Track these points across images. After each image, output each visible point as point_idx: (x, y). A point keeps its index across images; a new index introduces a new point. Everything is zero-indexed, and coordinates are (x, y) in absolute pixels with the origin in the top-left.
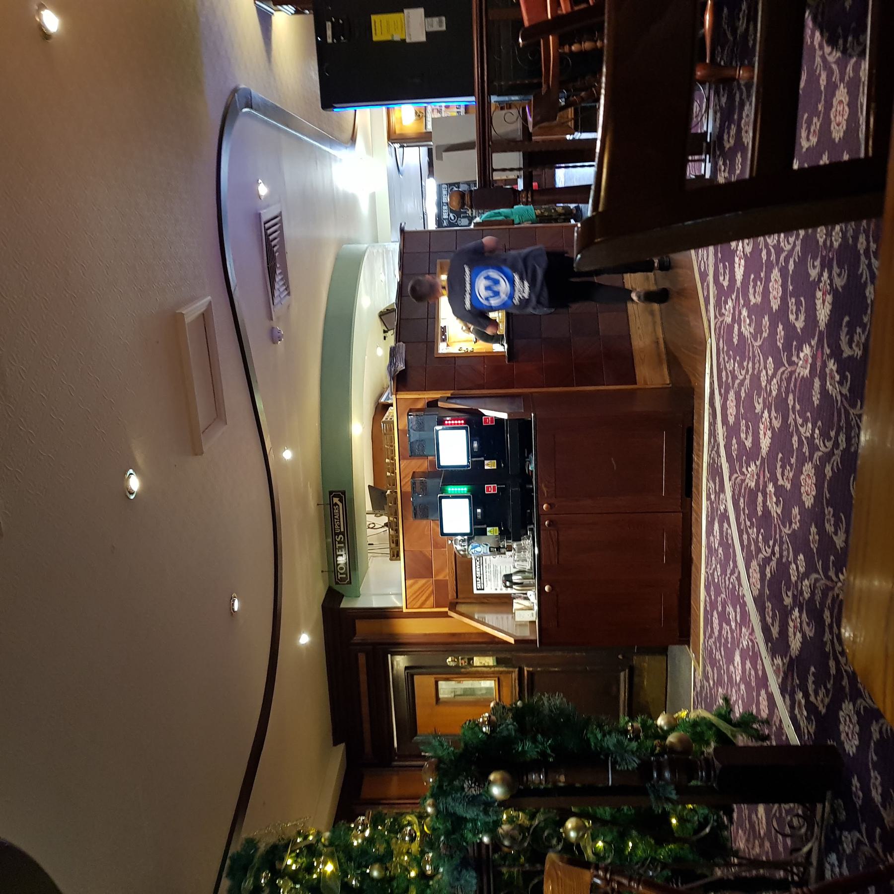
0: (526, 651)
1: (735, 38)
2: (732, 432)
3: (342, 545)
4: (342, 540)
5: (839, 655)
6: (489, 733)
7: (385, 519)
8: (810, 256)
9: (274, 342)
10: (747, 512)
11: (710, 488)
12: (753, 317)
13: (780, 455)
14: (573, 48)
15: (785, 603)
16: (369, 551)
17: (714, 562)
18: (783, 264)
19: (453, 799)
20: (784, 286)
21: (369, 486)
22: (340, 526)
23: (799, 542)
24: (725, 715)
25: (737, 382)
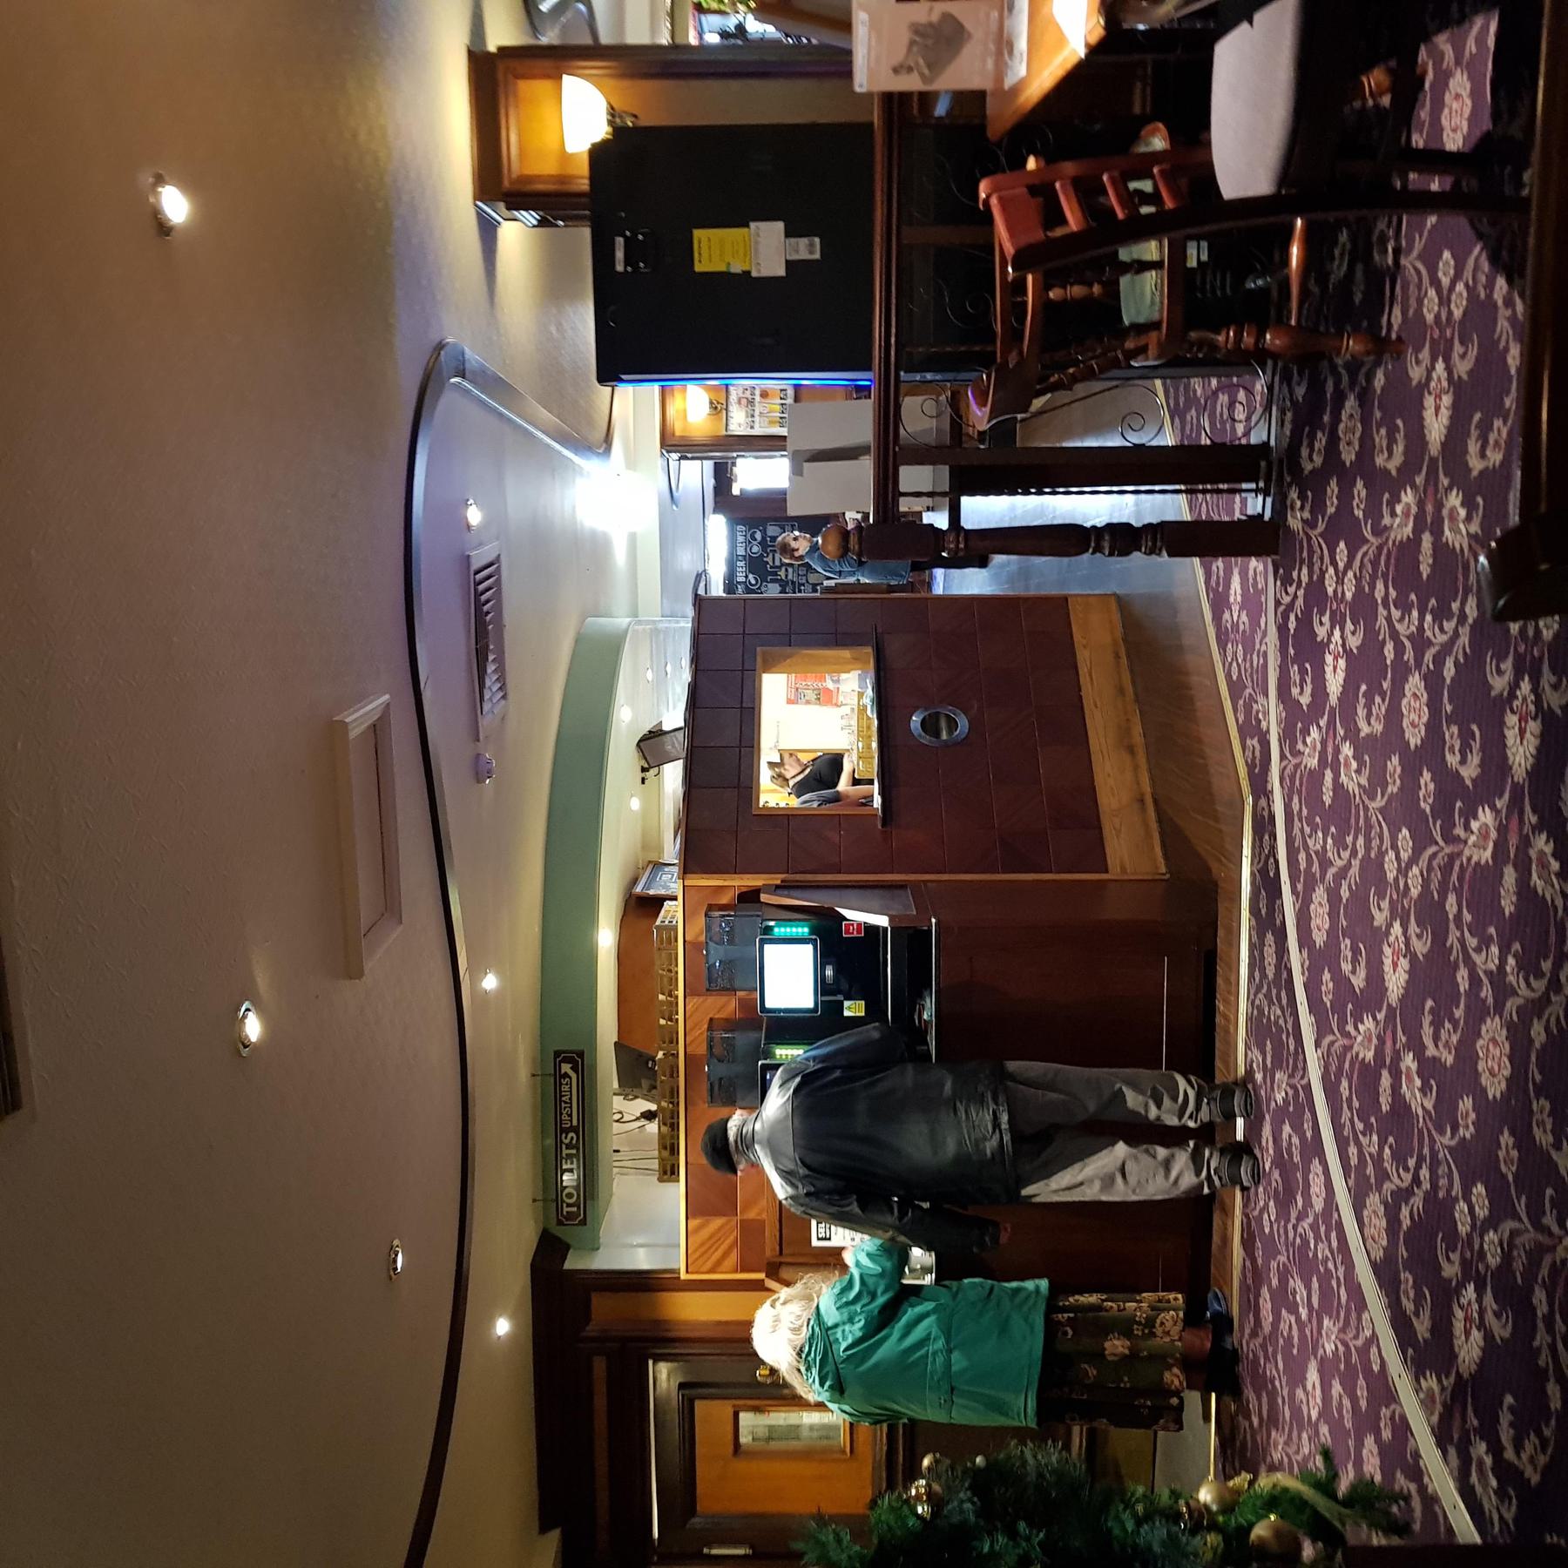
1: (1324, 289)
2: (1321, 959)
3: (574, 1151)
4: (574, 1142)
5: (1360, 1136)
6: (929, 1517)
8: (1489, 654)
9: (479, 779)
10: (1356, 1104)
11: (1252, 1061)
12: (1367, 758)
13: (1429, 1003)
14: (1051, 295)
15: (1445, 1274)
18: (1431, 666)
20: (1434, 705)
22: (570, 1115)
24: (1326, 1486)
25: (1331, 872)
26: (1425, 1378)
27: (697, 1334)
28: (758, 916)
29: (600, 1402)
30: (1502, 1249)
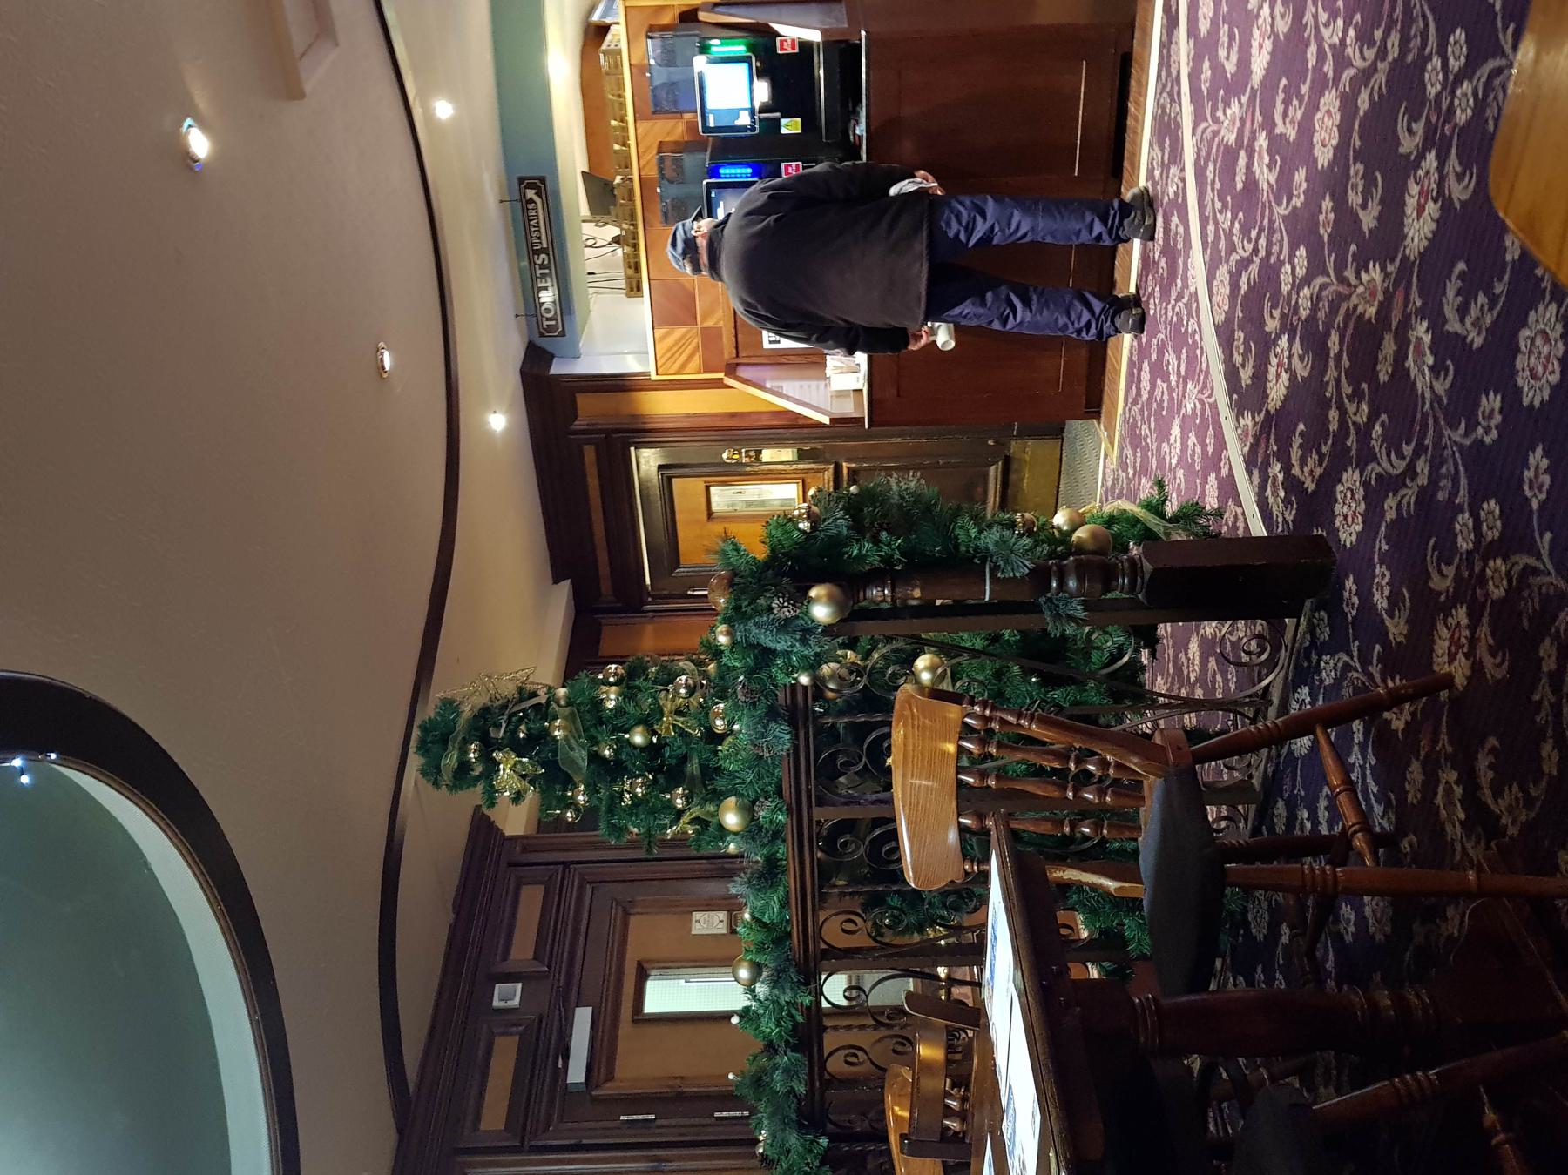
0: (847, 437)
2: (1204, 47)
3: (547, 271)
4: (546, 262)
5: (1346, 401)
7: (613, 231)
11: (1153, 159)
13: (1284, 82)
15: (1267, 329)
16: (590, 285)
17: (1150, 283)
19: (756, 624)
21: (583, 172)
23: (1302, 229)
24: (1156, 508)
28: (696, 35)
29: (593, 483)
30: (1510, 581)
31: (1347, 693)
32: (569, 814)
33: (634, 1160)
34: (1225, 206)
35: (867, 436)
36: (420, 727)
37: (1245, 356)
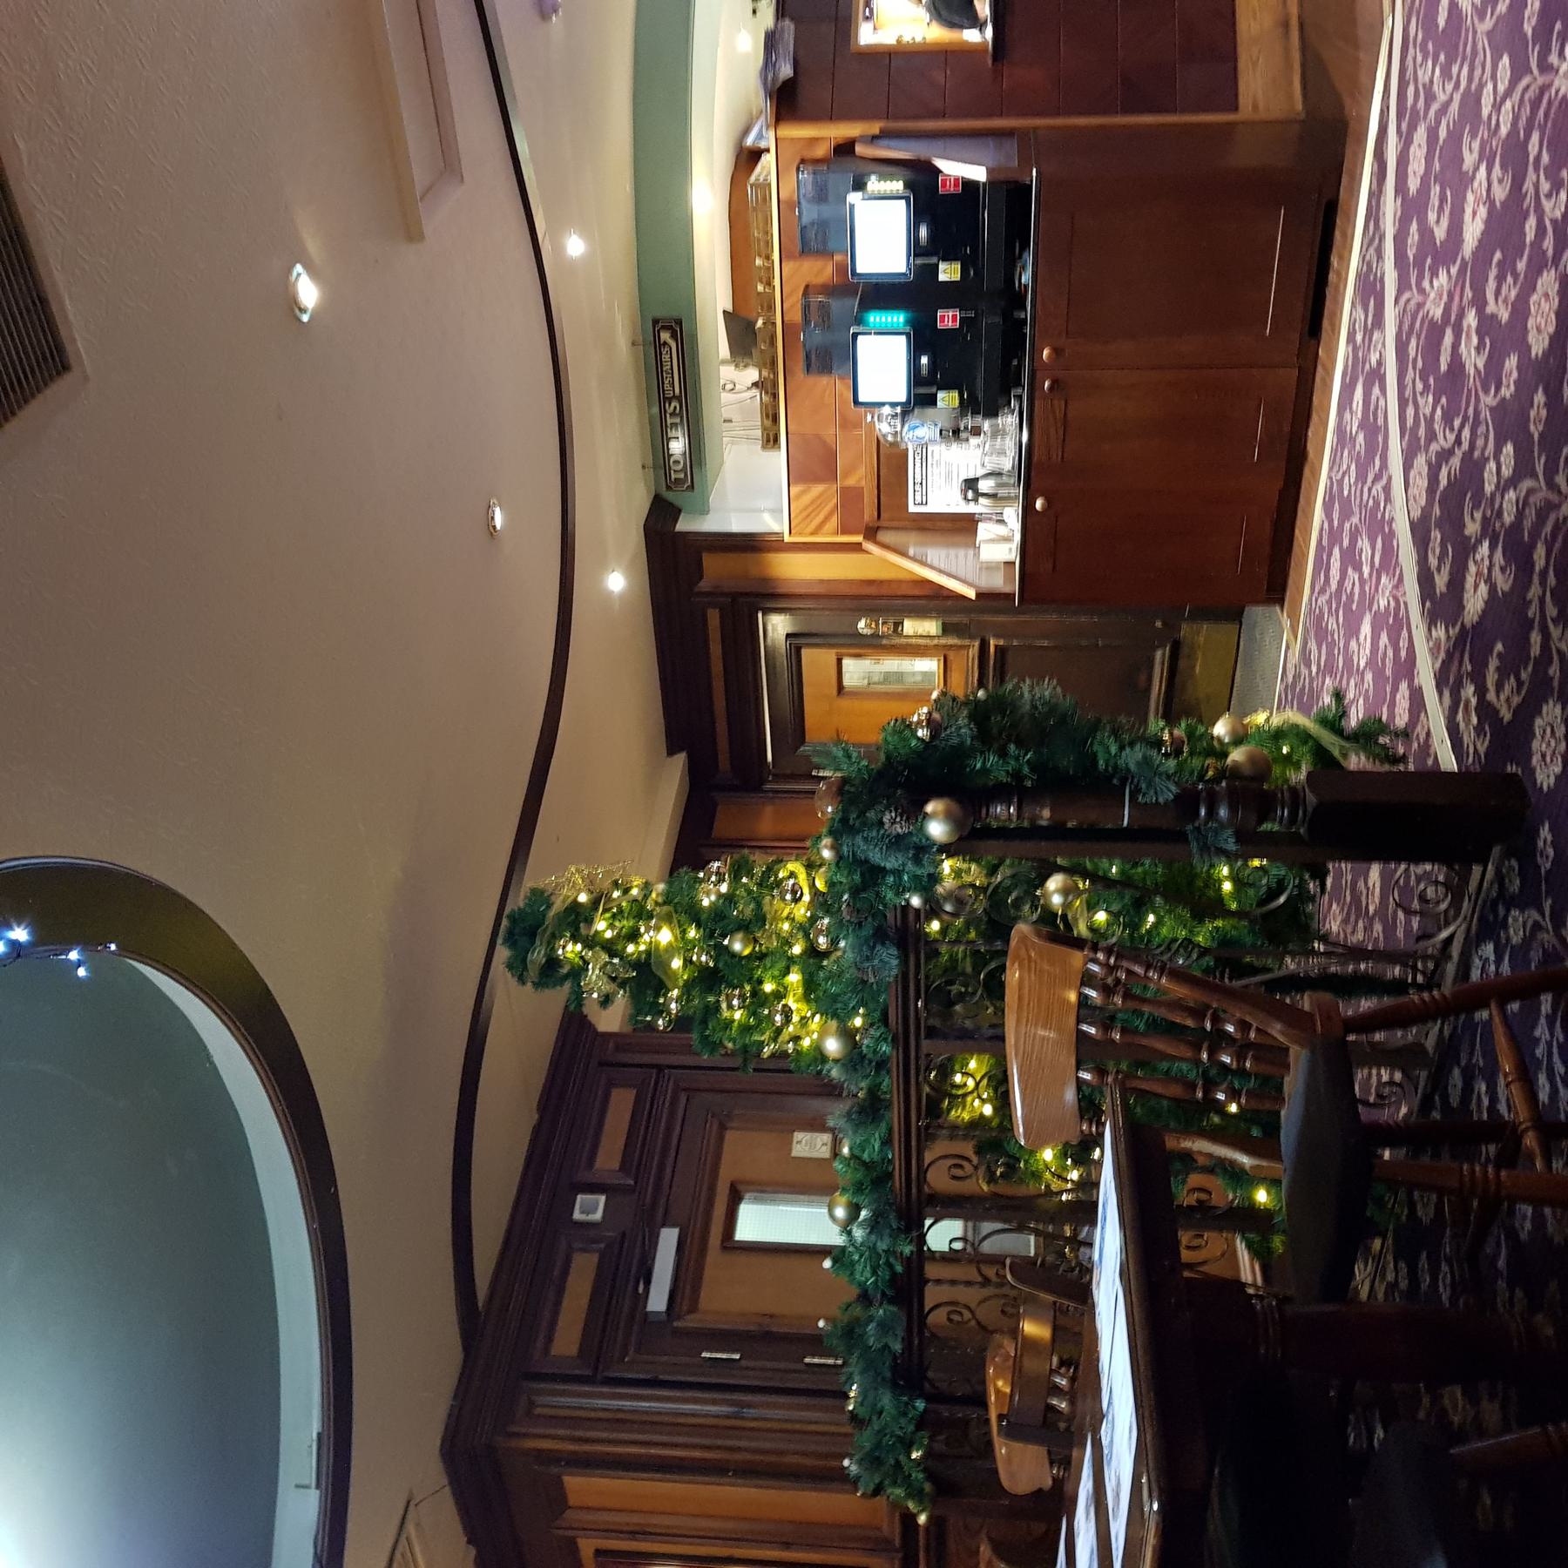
2: (1413, 208)
3: (678, 420)
7: (752, 374)
13: (1498, 255)
15: (1467, 532)
19: (865, 839)
23: (1510, 422)
24: (1334, 723)
26: (1437, 630)
27: (802, 591)
29: (716, 649)
31: (1535, 956)
32: (660, 1022)
33: (714, 1402)
34: (1426, 387)
35: (1018, 611)
36: (508, 916)
37: (1441, 559)
